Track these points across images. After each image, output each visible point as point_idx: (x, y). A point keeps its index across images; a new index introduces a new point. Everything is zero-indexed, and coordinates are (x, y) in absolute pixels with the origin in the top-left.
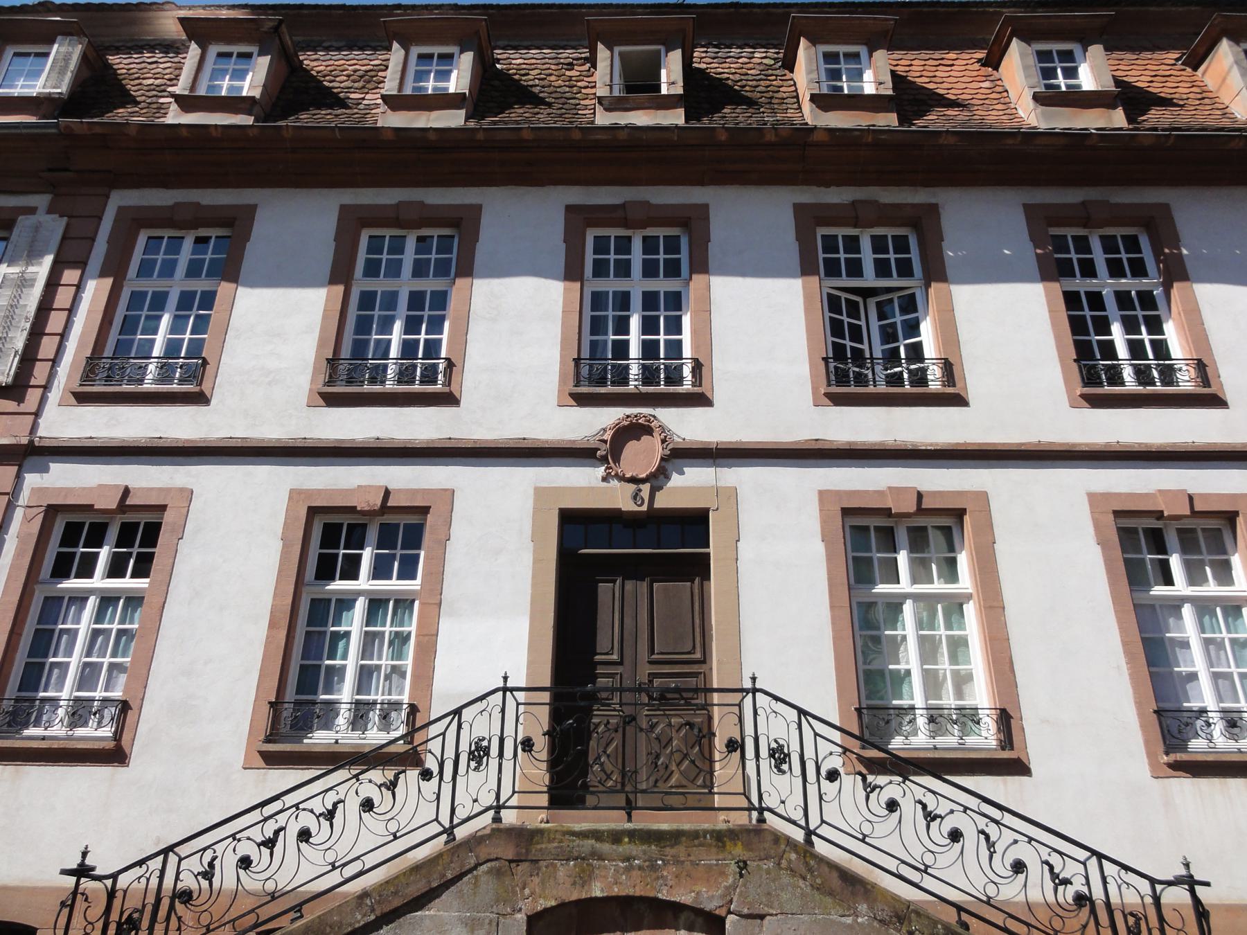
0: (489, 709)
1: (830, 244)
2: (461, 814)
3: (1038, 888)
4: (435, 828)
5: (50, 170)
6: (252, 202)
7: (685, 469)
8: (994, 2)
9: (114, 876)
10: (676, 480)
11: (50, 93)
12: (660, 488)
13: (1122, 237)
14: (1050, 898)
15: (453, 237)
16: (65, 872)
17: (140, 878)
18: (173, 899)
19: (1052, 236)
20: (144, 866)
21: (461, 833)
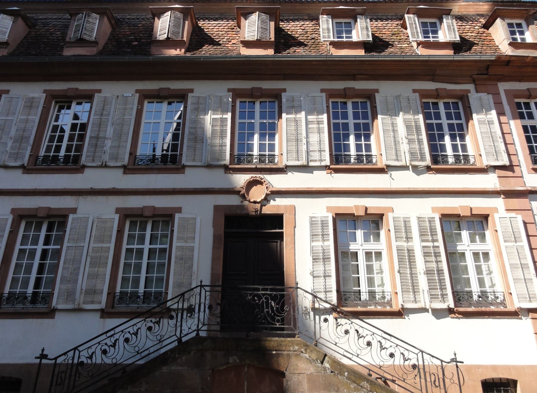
0: (195, 294)
1: (519, 105)
2: (184, 333)
3: (398, 360)
4: (175, 338)
5: (478, 74)
6: (99, 88)
7: (276, 199)
8: (328, 1)
9: (56, 359)
10: (272, 203)
11: (454, 41)
12: (265, 205)
13: (523, 103)
14: (402, 363)
15: (366, 102)
16: (36, 358)
17: (65, 360)
18: (77, 367)
19: (516, 103)
20: (66, 355)
21: (184, 339)
